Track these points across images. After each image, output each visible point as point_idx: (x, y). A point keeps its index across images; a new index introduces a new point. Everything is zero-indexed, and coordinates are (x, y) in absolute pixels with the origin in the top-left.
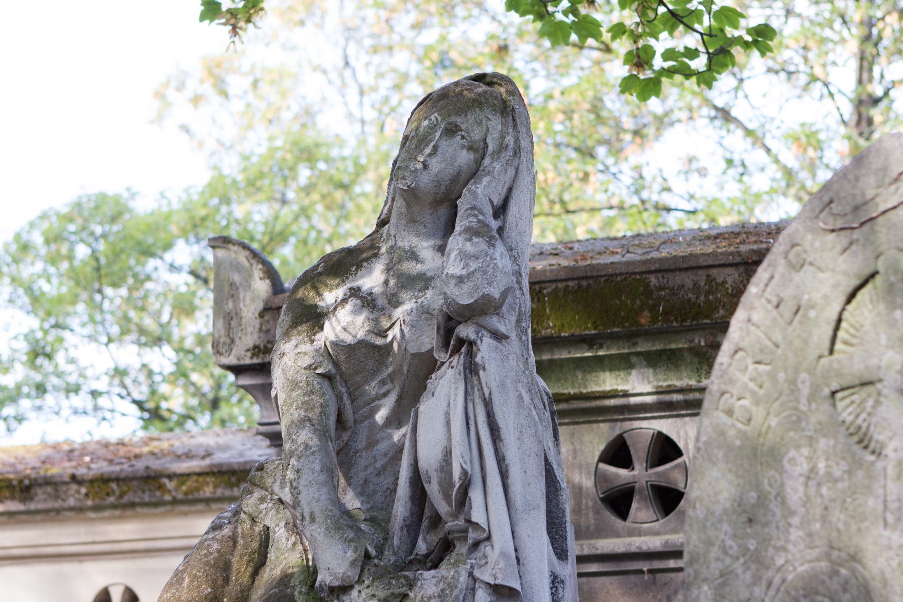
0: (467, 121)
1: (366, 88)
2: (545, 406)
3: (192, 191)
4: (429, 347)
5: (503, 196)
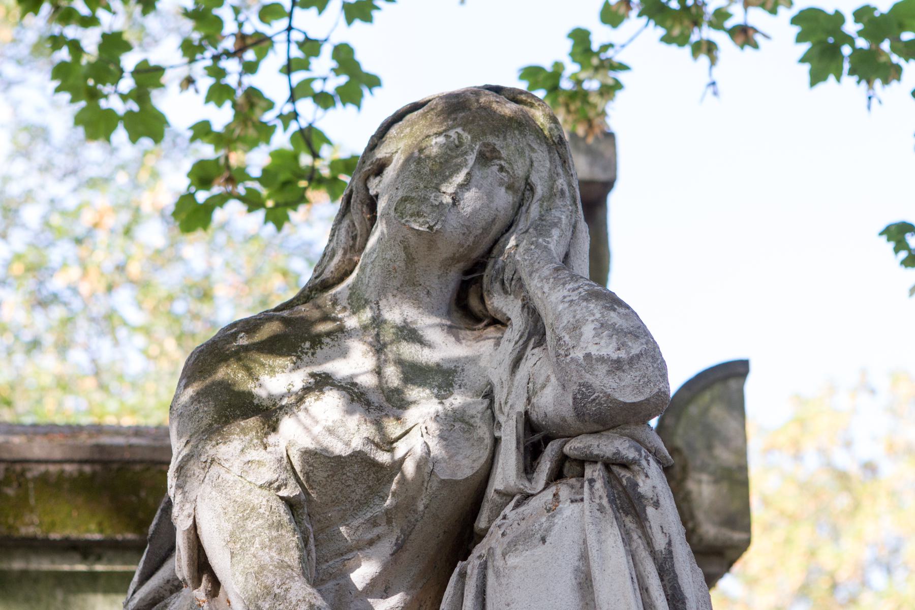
0: (508, 146)
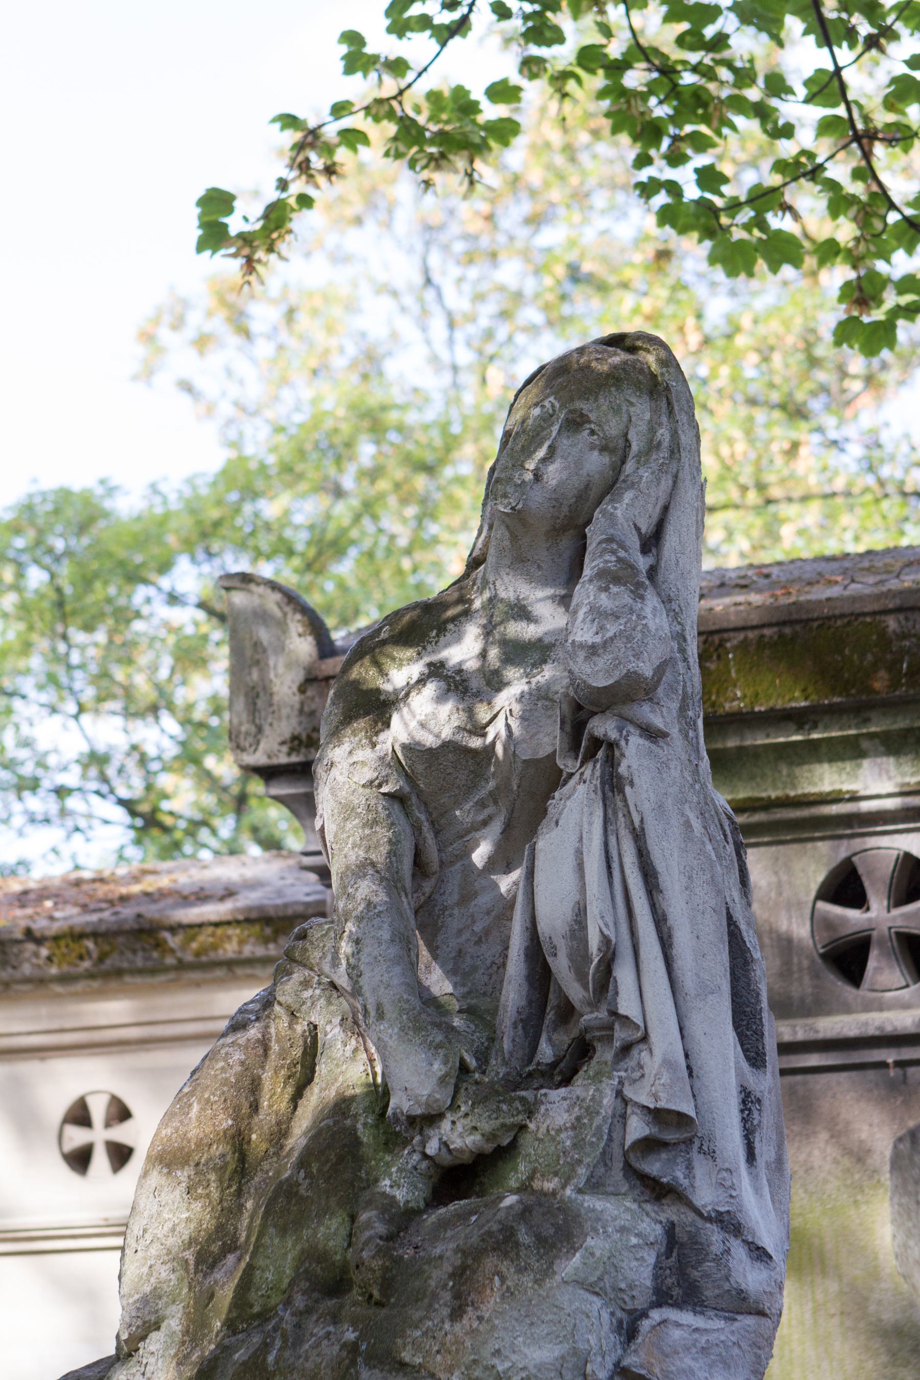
0: (598, 407)
1: (458, 318)
2: (725, 836)
3: (199, 482)
4: (549, 750)
5: (655, 519)
